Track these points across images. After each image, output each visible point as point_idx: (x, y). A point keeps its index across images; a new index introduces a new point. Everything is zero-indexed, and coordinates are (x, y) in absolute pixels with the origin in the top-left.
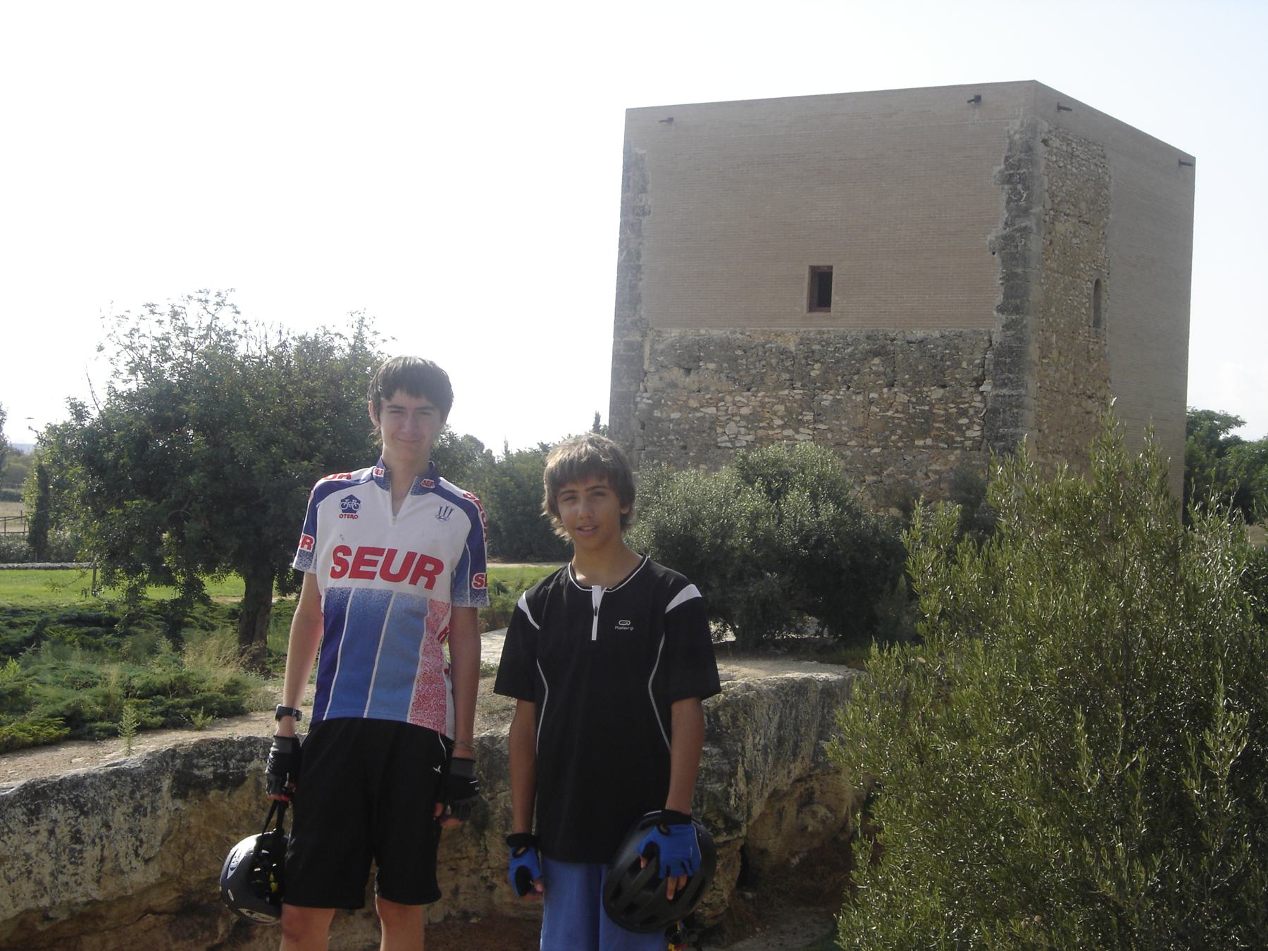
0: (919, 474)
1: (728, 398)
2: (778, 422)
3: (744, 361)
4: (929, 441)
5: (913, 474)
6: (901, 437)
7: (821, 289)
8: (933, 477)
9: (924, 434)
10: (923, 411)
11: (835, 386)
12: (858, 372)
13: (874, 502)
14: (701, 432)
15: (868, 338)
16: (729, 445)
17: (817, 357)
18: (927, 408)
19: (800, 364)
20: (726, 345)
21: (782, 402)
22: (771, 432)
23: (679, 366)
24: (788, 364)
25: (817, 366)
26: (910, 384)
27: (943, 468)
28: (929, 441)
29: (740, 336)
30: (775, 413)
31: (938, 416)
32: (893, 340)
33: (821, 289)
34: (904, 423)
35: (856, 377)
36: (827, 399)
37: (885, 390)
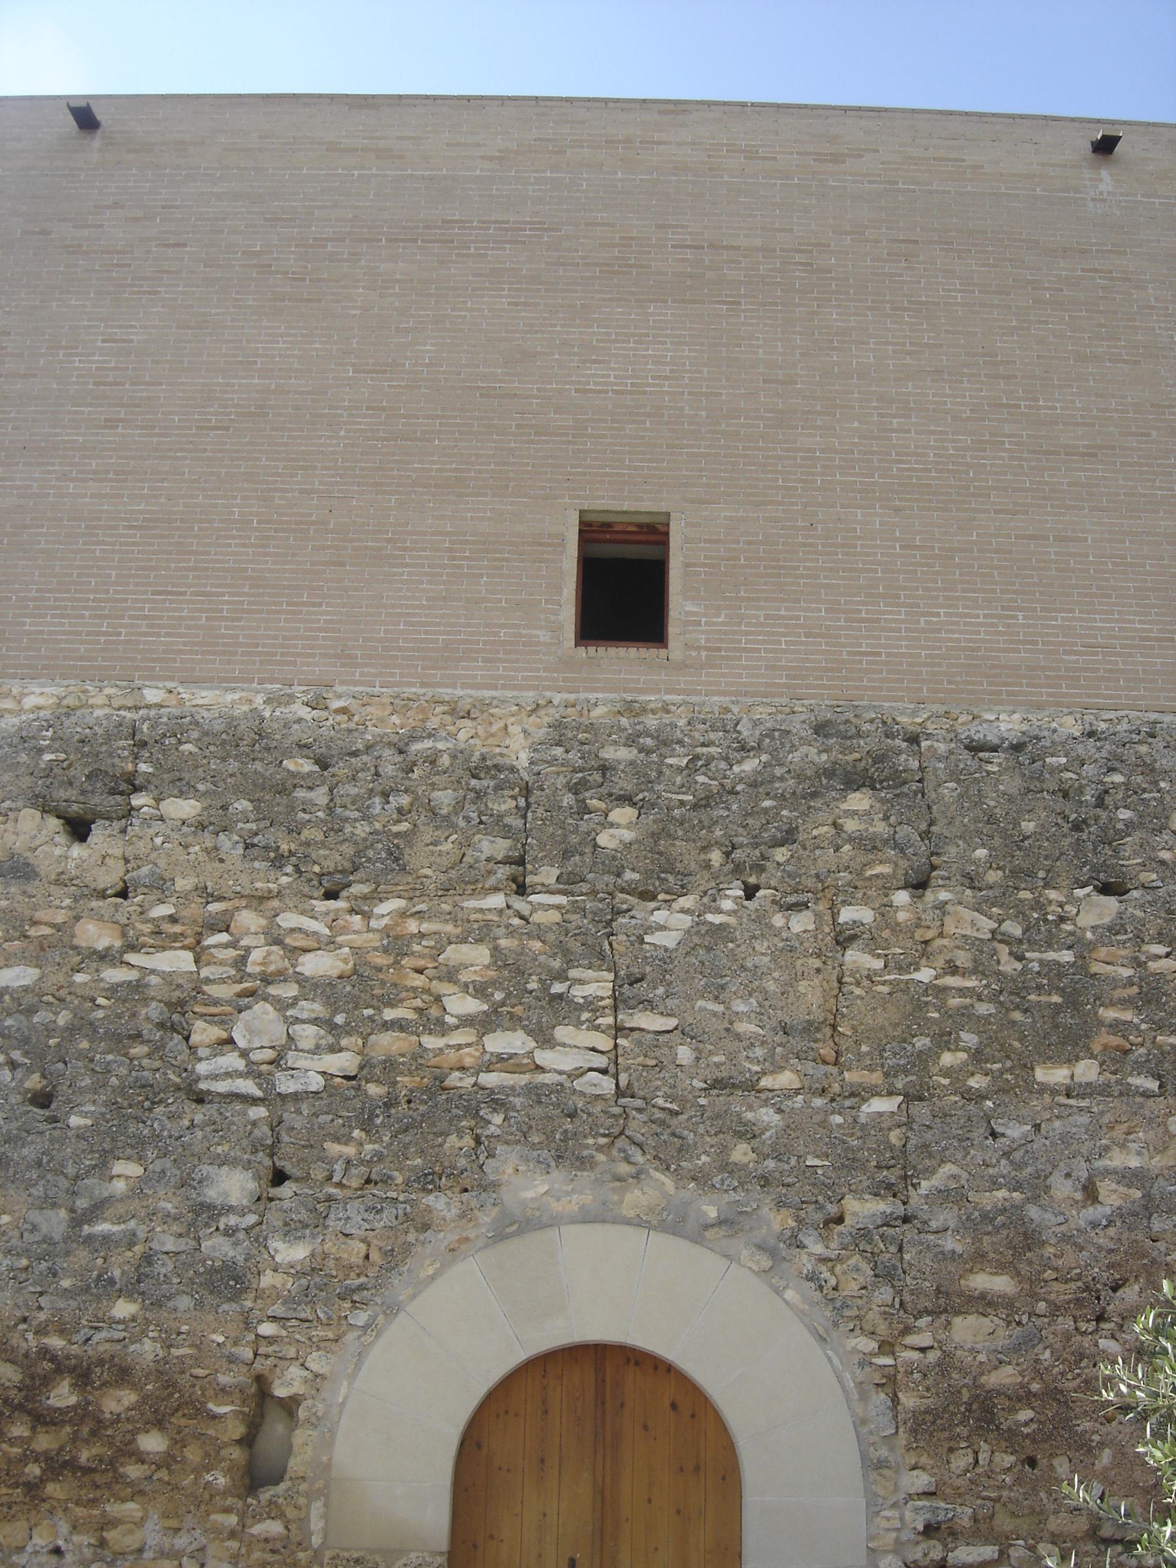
0: (1062, 1189)
1: (248, 920)
2: (461, 1005)
3: (320, 796)
4: (1087, 1071)
5: (1038, 1188)
6: (978, 1056)
7: (623, 590)
8: (1112, 1196)
9: (1071, 1045)
10: (1054, 970)
11: (703, 880)
12: (788, 837)
13: (885, 1294)
14: (122, 1040)
15: (821, 729)
16: (248, 1086)
17: (623, 783)
18: (1067, 956)
19: (553, 807)
20: (247, 742)
21: (482, 933)
22: (431, 1042)
23: (46, 808)
24: (504, 805)
25: (623, 814)
26: (993, 876)
27: (1158, 1162)
28: (1087, 1071)
29: (305, 713)
30: (450, 975)
31: (1115, 983)
32: (913, 740)
33: (623, 590)
34: (984, 1009)
35: (781, 854)
36: (669, 925)
37: (902, 897)
